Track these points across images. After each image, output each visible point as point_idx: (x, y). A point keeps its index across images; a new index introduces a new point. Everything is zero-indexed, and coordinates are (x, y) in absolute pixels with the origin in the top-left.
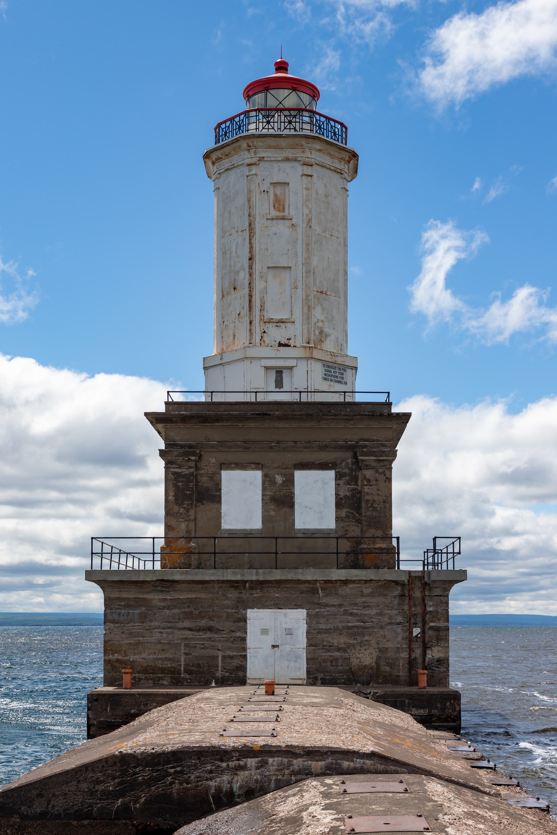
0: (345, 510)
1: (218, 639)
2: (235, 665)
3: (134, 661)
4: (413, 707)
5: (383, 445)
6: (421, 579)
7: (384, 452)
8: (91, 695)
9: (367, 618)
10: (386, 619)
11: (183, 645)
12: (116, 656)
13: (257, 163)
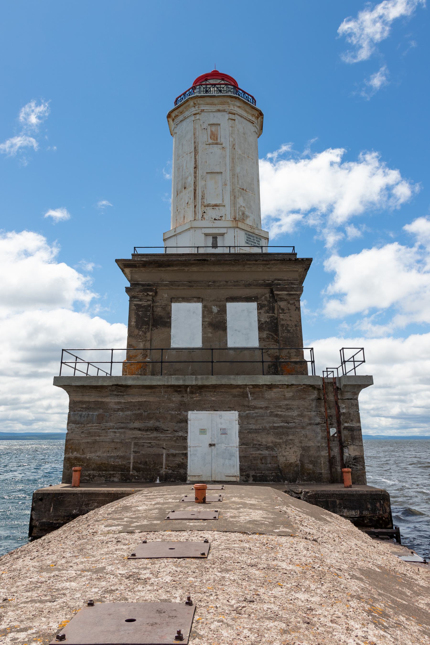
0: (266, 332)
1: (163, 438)
2: (177, 462)
3: (90, 459)
4: (344, 508)
5: (292, 284)
7: (293, 288)
8: (37, 494)
9: (289, 419)
10: (306, 420)
11: (133, 444)
12: (75, 454)
13: (200, 113)
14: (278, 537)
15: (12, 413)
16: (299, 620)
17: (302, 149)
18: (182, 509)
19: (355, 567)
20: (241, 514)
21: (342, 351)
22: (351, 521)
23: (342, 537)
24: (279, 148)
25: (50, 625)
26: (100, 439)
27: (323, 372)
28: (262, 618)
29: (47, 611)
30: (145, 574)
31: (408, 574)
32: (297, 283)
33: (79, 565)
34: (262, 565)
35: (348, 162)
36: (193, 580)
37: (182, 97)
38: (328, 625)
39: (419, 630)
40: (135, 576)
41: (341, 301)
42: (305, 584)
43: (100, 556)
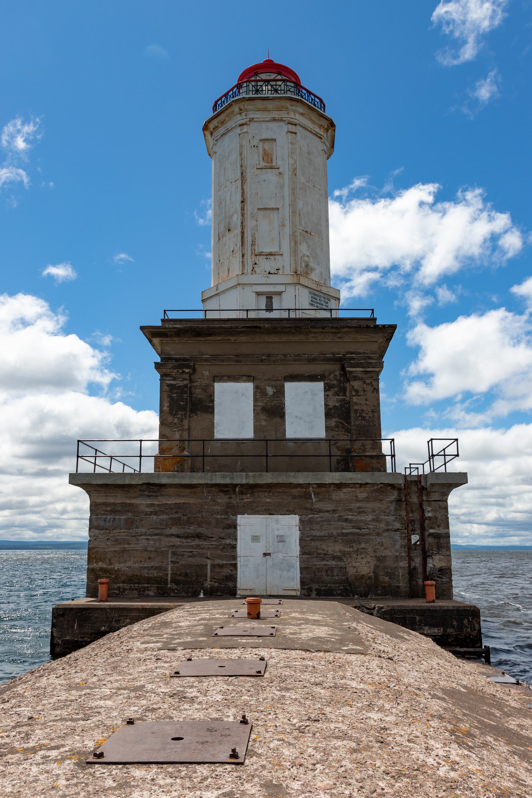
1: (207, 546)
2: (225, 574)
3: (119, 570)
4: (425, 625)
5: (369, 358)
6: (417, 484)
7: (371, 363)
9: (362, 524)
10: (383, 526)
11: (170, 553)
13: (248, 123)
14: (347, 655)
15: (18, 519)
16: (372, 739)
17: (382, 187)
18: (232, 625)
19: (437, 687)
20: (302, 631)
21: (430, 442)
22: (432, 639)
23: (421, 656)
24: (352, 183)
25: (85, 743)
26: (130, 547)
27: (405, 468)
28: (328, 737)
29: (80, 729)
30: (192, 693)
31: (498, 695)
32: (376, 358)
33: (114, 683)
34: (329, 684)
35: (442, 202)
36: (248, 698)
37: (223, 99)
38: (404, 744)
39: (509, 751)
40: (180, 694)
41: (427, 383)
42: (378, 704)
43: (138, 674)
